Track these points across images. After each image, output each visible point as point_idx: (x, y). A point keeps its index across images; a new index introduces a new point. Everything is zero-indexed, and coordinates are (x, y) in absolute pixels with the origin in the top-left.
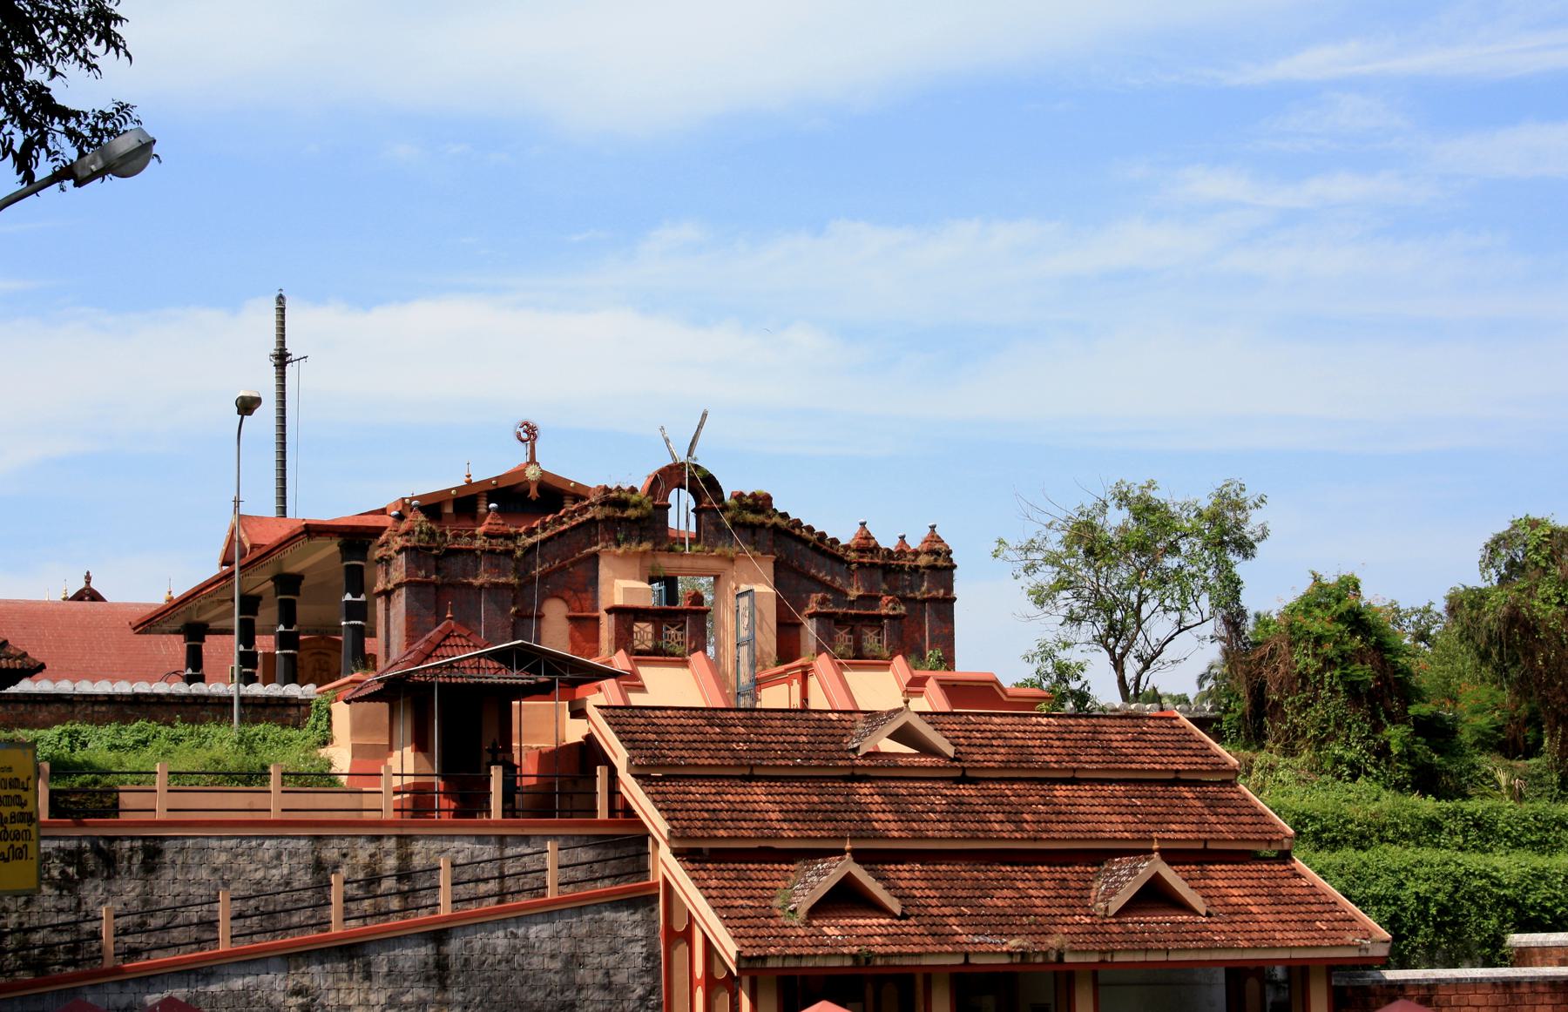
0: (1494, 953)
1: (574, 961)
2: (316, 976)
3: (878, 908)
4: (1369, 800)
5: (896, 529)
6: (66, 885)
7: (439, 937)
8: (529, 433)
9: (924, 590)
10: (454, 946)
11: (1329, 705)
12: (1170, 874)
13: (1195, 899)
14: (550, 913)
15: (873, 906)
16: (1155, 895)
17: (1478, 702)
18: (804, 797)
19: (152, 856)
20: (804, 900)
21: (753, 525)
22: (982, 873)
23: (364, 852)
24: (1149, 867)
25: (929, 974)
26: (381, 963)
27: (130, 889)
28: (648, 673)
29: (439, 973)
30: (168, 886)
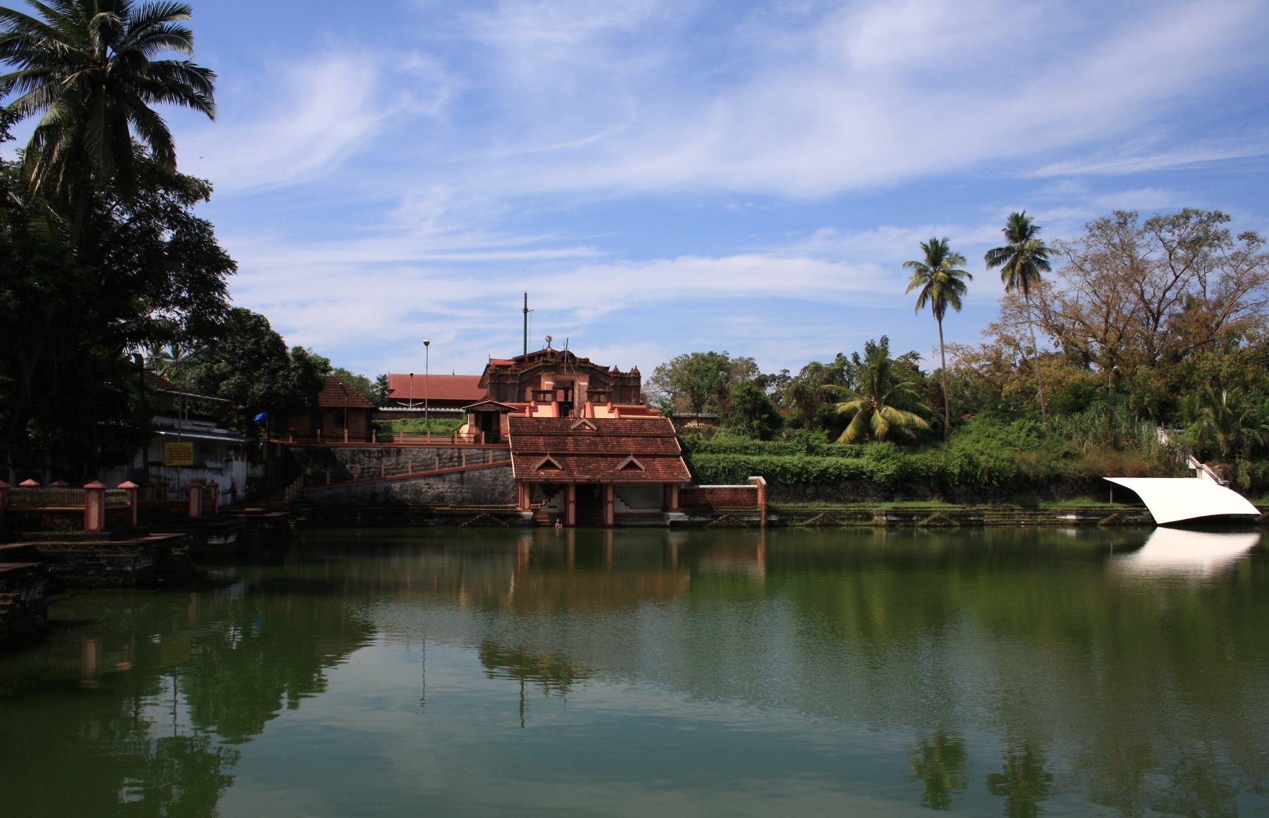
0: (745, 481)
1: (495, 479)
2: (431, 481)
3: (556, 468)
4: (746, 440)
5: (625, 369)
6: (379, 458)
7: (462, 472)
8: (549, 339)
9: (632, 383)
10: (465, 475)
11: (739, 415)
12: (635, 460)
13: (642, 467)
14: (489, 468)
15: (555, 467)
16: (631, 465)
17: (791, 411)
18: (553, 440)
19: (399, 452)
20: (537, 466)
21: (585, 367)
22: (587, 459)
23: (450, 452)
24: (628, 460)
25: (607, 485)
26: (447, 478)
27: (393, 460)
28: (540, 407)
29: (461, 481)
30: (402, 459)
